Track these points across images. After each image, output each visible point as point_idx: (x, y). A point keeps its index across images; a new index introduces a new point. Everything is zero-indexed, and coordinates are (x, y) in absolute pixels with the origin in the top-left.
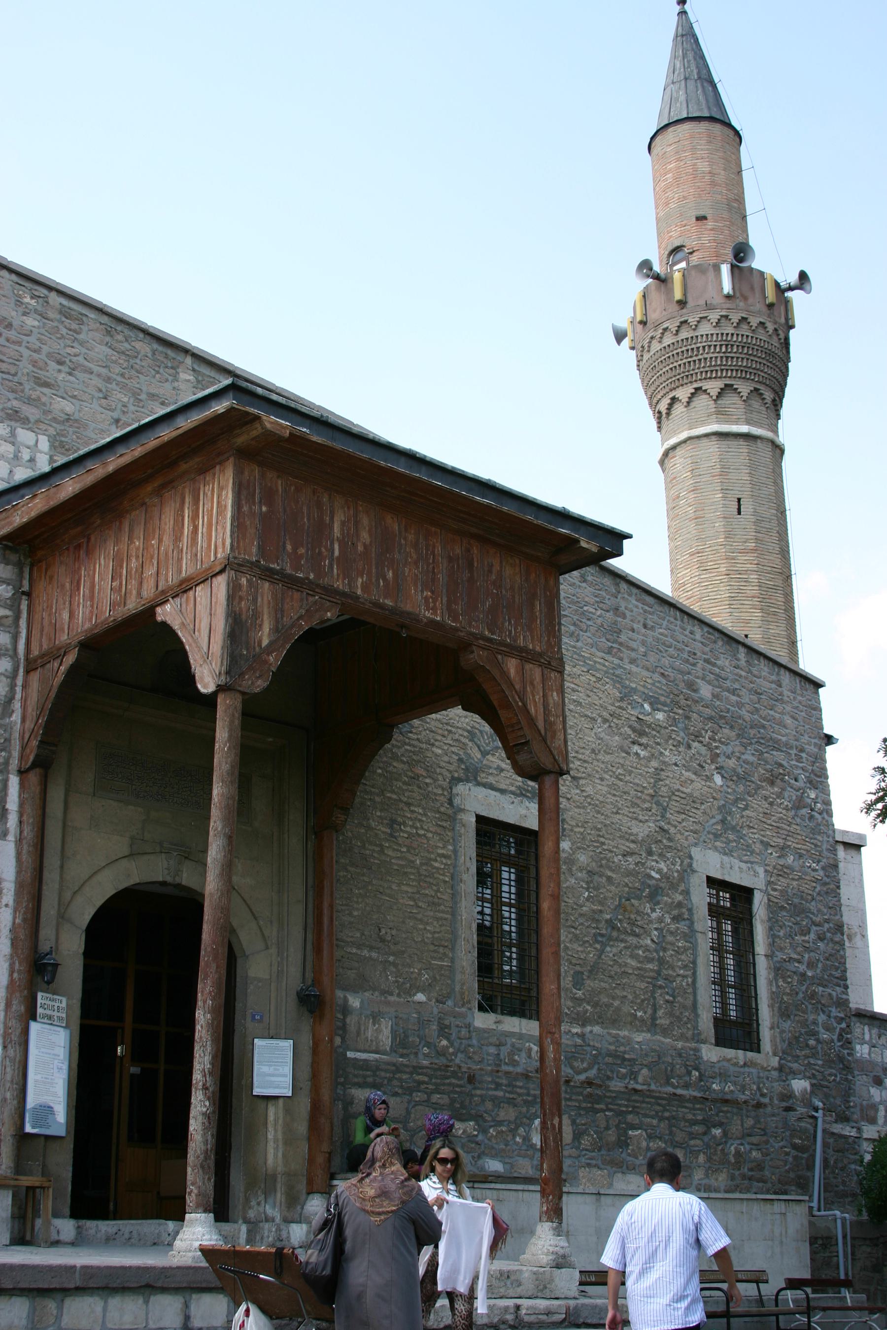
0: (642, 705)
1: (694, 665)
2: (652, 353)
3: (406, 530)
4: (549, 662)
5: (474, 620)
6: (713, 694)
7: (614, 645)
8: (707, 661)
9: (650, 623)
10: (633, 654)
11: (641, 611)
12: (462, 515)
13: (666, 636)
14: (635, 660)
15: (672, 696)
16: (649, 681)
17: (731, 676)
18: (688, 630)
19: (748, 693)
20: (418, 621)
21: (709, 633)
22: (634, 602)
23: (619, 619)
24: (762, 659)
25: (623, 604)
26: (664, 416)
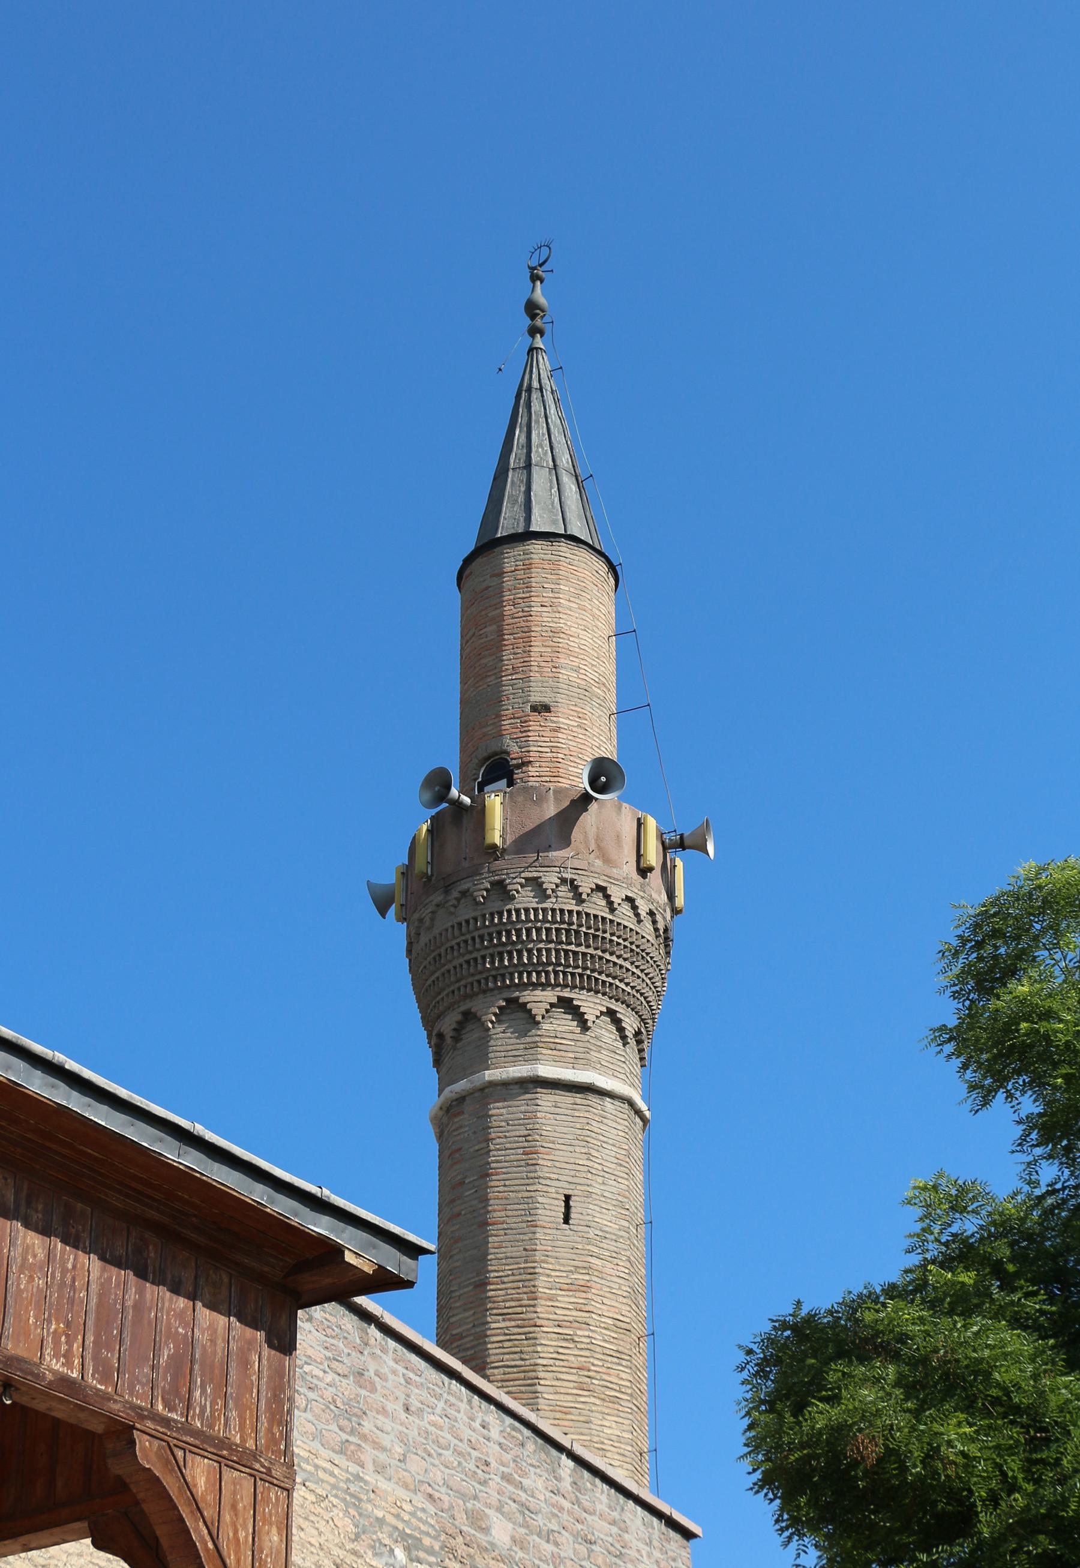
0: (392, 1551)
1: (484, 1483)
2: (436, 931)
3: (28, 1204)
4: (269, 1469)
5: (139, 1382)
6: (514, 1540)
7: (352, 1439)
8: (507, 1478)
9: (415, 1404)
10: (383, 1457)
11: (403, 1381)
12: (134, 1184)
13: (441, 1428)
14: (385, 1467)
15: (443, 1537)
16: (407, 1507)
17: (545, 1509)
18: (479, 1421)
19: (571, 1539)
20: (38, 1377)
21: (514, 1429)
22: (392, 1363)
23: (363, 1392)
24: (597, 1481)
25: (372, 1367)
26: (449, 1041)
